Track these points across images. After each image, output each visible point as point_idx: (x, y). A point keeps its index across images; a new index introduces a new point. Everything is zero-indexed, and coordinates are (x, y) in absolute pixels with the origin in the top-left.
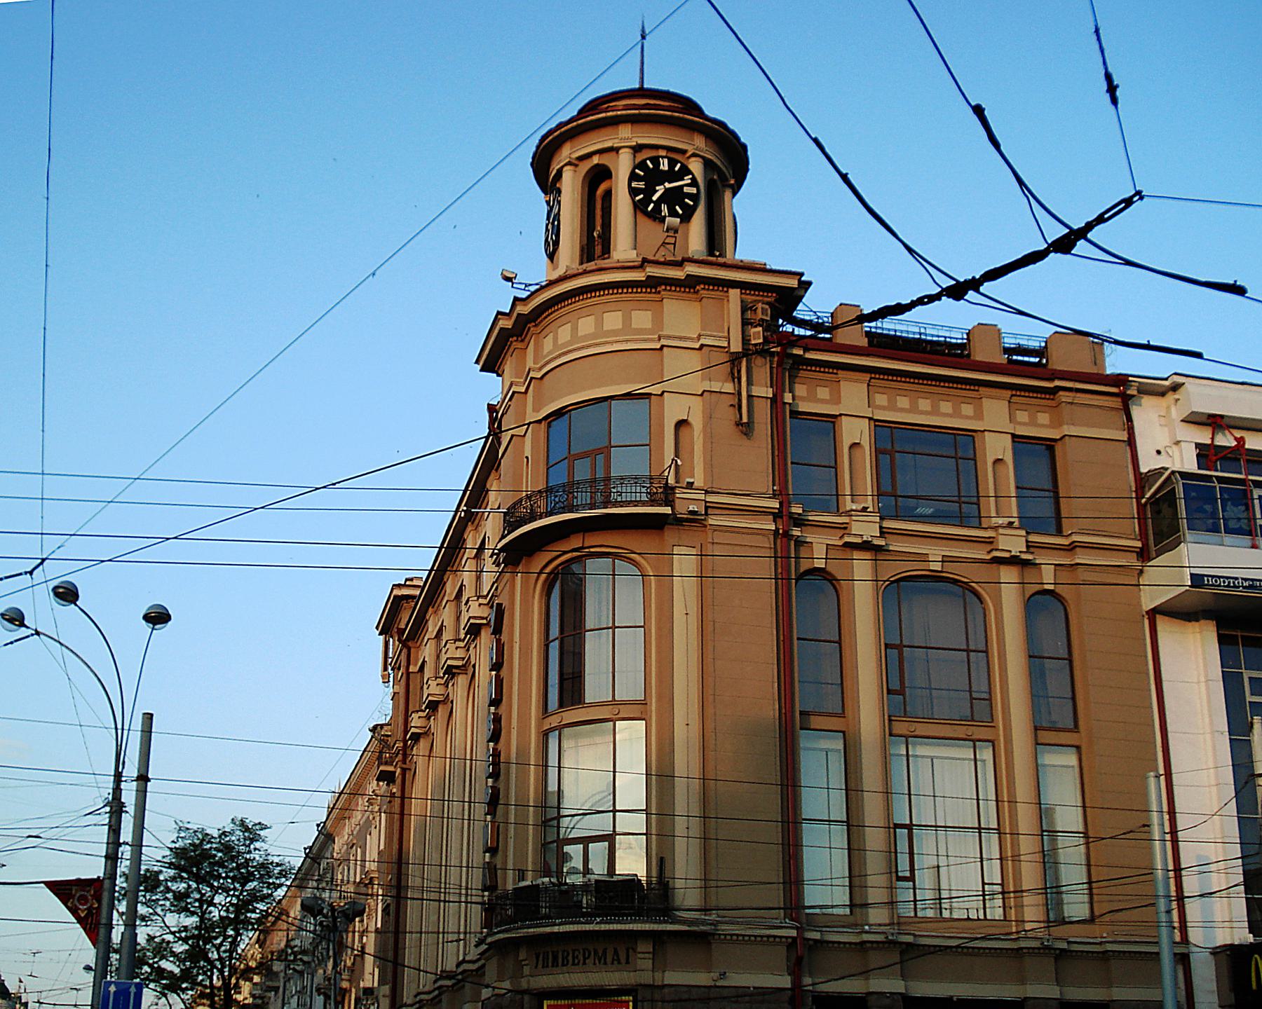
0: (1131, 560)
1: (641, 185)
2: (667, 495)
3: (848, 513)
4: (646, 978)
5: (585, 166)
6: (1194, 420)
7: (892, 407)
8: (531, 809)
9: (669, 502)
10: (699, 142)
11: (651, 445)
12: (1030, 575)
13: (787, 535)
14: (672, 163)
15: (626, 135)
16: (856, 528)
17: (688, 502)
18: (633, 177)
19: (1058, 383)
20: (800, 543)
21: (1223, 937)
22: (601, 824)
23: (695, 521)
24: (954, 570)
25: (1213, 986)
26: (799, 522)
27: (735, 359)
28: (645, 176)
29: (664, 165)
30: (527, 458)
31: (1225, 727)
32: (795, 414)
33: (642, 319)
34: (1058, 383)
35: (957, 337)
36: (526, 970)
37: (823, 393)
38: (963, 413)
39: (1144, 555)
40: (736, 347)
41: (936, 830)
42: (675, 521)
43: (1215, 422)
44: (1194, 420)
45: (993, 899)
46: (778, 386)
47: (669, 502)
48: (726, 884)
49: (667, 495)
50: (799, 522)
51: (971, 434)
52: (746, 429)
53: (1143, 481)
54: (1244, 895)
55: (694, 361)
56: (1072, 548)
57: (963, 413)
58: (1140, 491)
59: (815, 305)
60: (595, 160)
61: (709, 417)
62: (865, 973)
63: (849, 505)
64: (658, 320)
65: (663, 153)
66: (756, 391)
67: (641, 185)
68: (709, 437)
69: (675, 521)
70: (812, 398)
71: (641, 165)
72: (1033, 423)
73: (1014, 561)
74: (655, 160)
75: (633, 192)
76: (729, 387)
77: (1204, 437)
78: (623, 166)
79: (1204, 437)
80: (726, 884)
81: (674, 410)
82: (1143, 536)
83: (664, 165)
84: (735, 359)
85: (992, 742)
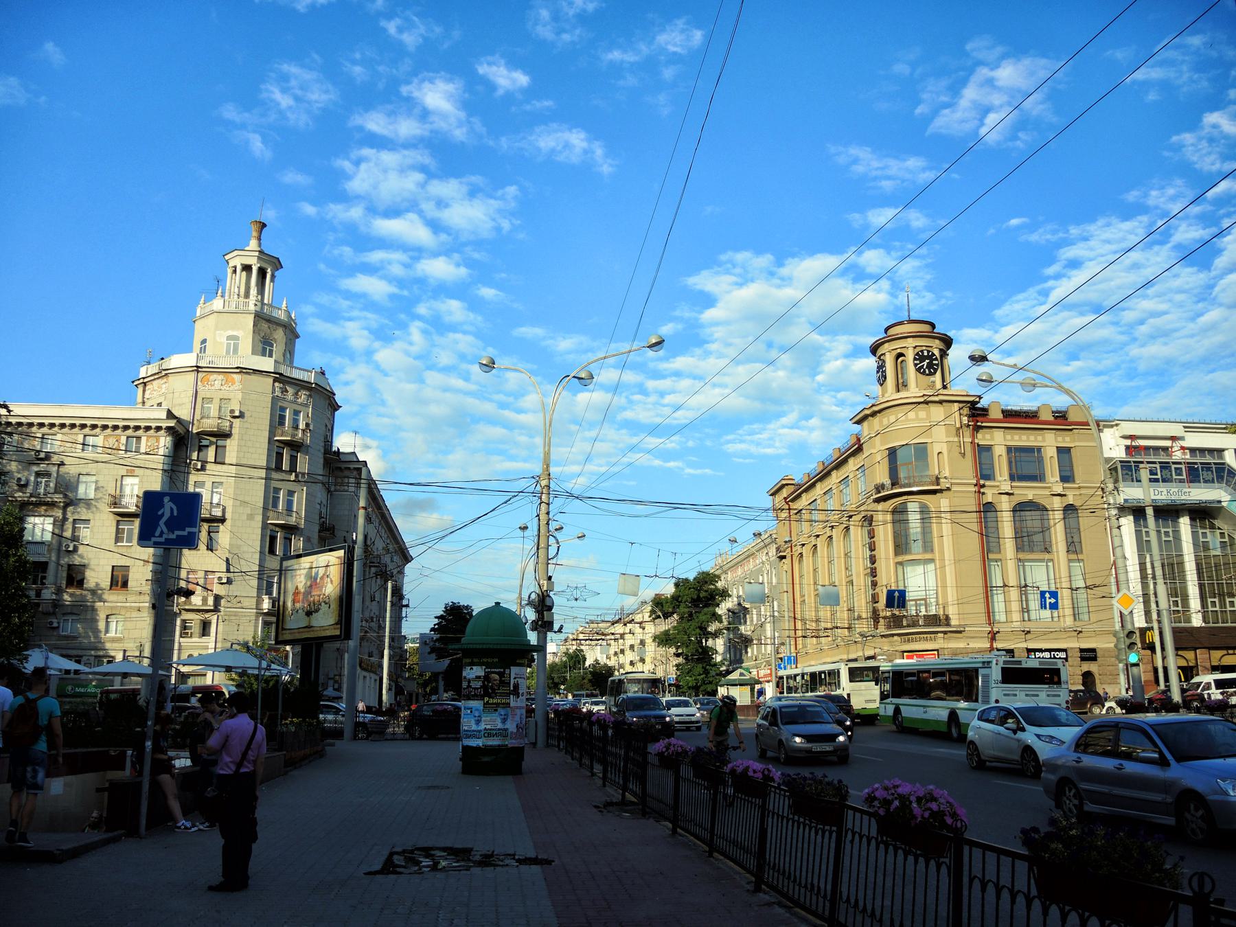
1: (934, 362)
5: (895, 353)
6: (1125, 437)
7: (1012, 440)
10: (937, 342)
13: (979, 492)
14: (928, 352)
15: (911, 342)
16: (1003, 487)
17: (944, 484)
19: (1073, 427)
20: (983, 493)
26: (983, 486)
27: (958, 429)
28: (920, 357)
29: (926, 354)
31: (1136, 551)
32: (978, 445)
33: (922, 414)
34: (1073, 427)
35: (1034, 409)
37: (988, 436)
40: (958, 425)
41: (1064, 616)
42: (941, 491)
43: (1132, 437)
44: (1125, 437)
46: (973, 437)
50: (983, 486)
51: (1039, 449)
52: (964, 455)
55: (1005, 519)
56: (1079, 488)
60: (899, 351)
61: (949, 451)
62: (77, 672)
63: (1000, 479)
64: (928, 415)
65: (924, 348)
66: (966, 440)
68: (950, 459)
69: (941, 491)
70: (984, 439)
71: (917, 354)
72: (1064, 441)
74: (922, 351)
76: (956, 439)
77: (1128, 442)
78: (910, 355)
79: (1128, 442)
83: (926, 354)
84: (958, 429)
85: (1052, 560)
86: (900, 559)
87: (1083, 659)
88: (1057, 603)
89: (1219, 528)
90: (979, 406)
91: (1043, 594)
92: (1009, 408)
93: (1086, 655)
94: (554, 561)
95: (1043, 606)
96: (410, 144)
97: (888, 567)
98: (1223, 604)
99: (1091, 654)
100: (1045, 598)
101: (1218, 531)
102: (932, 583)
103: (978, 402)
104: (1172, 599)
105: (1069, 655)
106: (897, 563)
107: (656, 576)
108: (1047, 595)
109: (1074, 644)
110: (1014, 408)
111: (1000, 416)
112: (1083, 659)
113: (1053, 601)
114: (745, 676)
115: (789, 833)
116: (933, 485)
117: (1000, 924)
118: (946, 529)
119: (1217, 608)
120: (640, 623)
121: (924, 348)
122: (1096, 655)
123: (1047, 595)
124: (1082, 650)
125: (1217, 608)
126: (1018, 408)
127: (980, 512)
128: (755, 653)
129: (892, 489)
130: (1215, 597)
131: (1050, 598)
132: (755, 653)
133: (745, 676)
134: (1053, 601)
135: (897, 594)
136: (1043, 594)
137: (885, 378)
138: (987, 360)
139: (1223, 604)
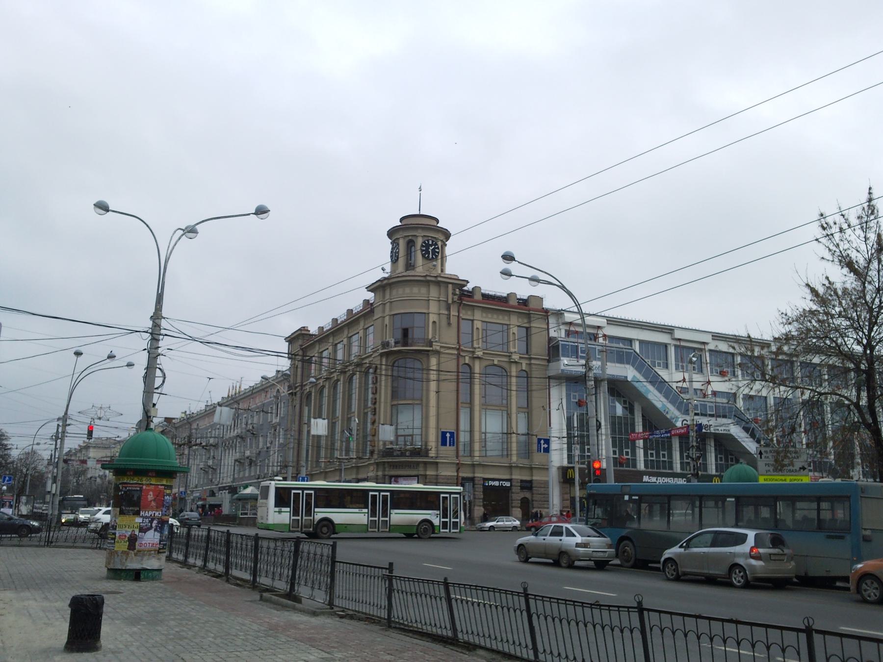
0: (545, 363)
1: (424, 249)
2: (430, 344)
3: (475, 348)
4: (422, 473)
5: (407, 239)
9: (431, 346)
11: (425, 327)
14: (433, 241)
17: (436, 346)
18: (422, 246)
21: (320, 421)
22: (410, 432)
24: (501, 364)
25: (536, 634)
30: (386, 325)
36: (387, 469)
38: (593, 562)
39: (549, 361)
49: (430, 344)
53: (550, 339)
57: (593, 562)
58: (549, 343)
59: (469, 287)
60: (410, 238)
65: (430, 238)
67: (424, 249)
74: (428, 241)
75: (422, 251)
76: (446, 313)
78: (419, 242)
83: (430, 243)
86: (395, 403)
87: (522, 488)
89: (623, 397)
90: (465, 288)
91: (539, 440)
92: (487, 292)
93: (525, 485)
94: (159, 391)
96: (879, 268)
97: (385, 407)
99: (528, 485)
100: (541, 444)
102: (418, 423)
103: (465, 286)
105: (513, 484)
106: (392, 405)
107: (249, 409)
108: (542, 442)
109: (517, 476)
111: (480, 298)
112: (522, 488)
113: (546, 446)
115: (484, 616)
117: (756, 660)
118: (383, 378)
119: (666, 459)
120: (181, 446)
121: (430, 238)
122: (531, 485)
123: (542, 442)
124: (522, 481)
125: (723, 462)
126: (494, 293)
127: (531, 377)
129: (395, 347)
130: (665, 451)
131: (544, 444)
132: (258, 473)
134: (546, 446)
135: (448, 435)
136: (539, 440)
137: (398, 258)
138: (514, 260)
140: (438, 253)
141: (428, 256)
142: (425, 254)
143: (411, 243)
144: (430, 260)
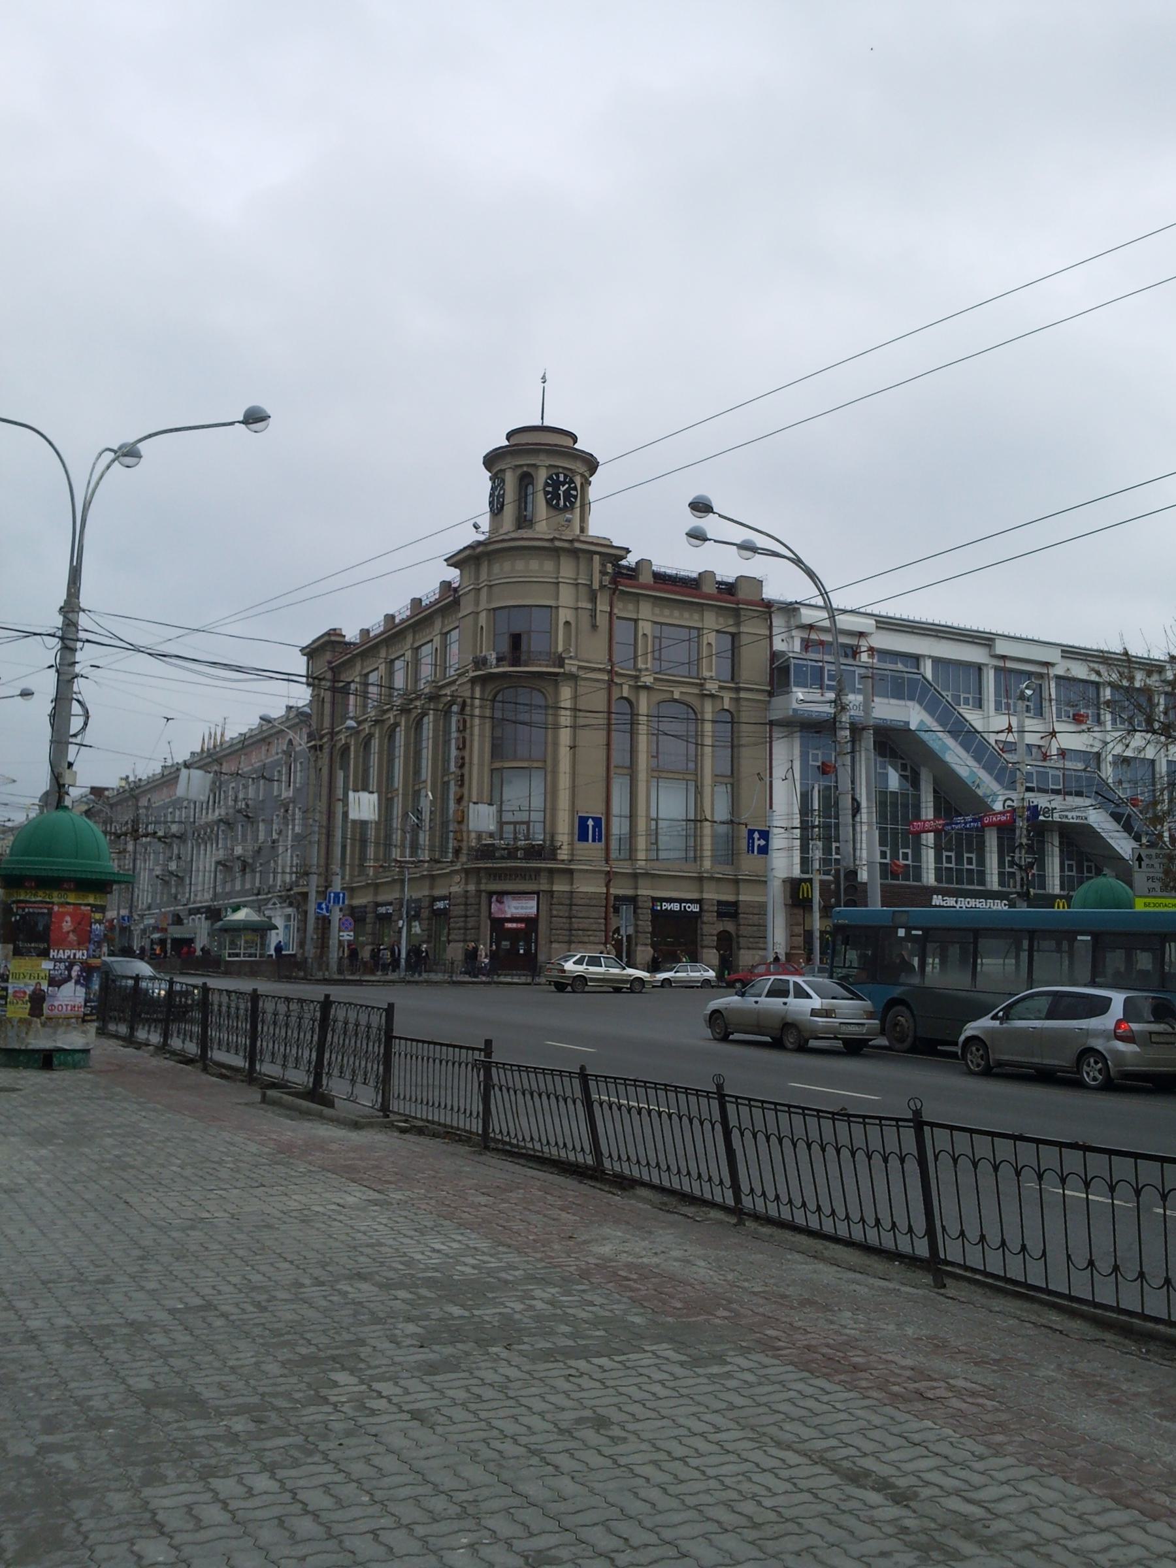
5: (519, 471)
8: (1168, 1213)
9: (562, 665)
12: (719, 702)
14: (566, 476)
18: (547, 484)
22: (524, 817)
23: (573, 677)
29: (562, 478)
36: (484, 881)
39: (771, 694)
45: (552, 540)
47: (562, 665)
48: (227, 621)
53: (774, 655)
54: (744, 931)
58: (772, 661)
59: (631, 560)
60: (525, 469)
67: (550, 489)
73: (712, 696)
74: (557, 475)
76: (589, 606)
78: (542, 476)
80: (227, 621)
81: (564, 615)
82: (771, 683)
83: (562, 478)
86: (497, 765)
87: (721, 915)
88: (767, 846)
89: (902, 758)
90: (624, 562)
91: (751, 832)
92: (662, 570)
93: (724, 909)
94: (78, 740)
95: (750, 849)
98: (959, 859)
99: (732, 910)
101: (900, 761)
102: (537, 802)
103: (623, 558)
104: (1067, 862)
105: (705, 907)
108: (756, 835)
109: (712, 894)
110: (669, 571)
111: (651, 580)
113: (762, 842)
114: (575, 963)
116: (554, 666)
123: (756, 835)
124: (720, 903)
128: (257, 884)
132: (257, 884)
133: (575, 963)
134: (762, 842)
135: (590, 823)
136: (751, 832)
139: (959, 859)
140: (575, 497)
141: (558, 504)
142: (552, 499)
143: (526, 480)
144: (561, 509)
